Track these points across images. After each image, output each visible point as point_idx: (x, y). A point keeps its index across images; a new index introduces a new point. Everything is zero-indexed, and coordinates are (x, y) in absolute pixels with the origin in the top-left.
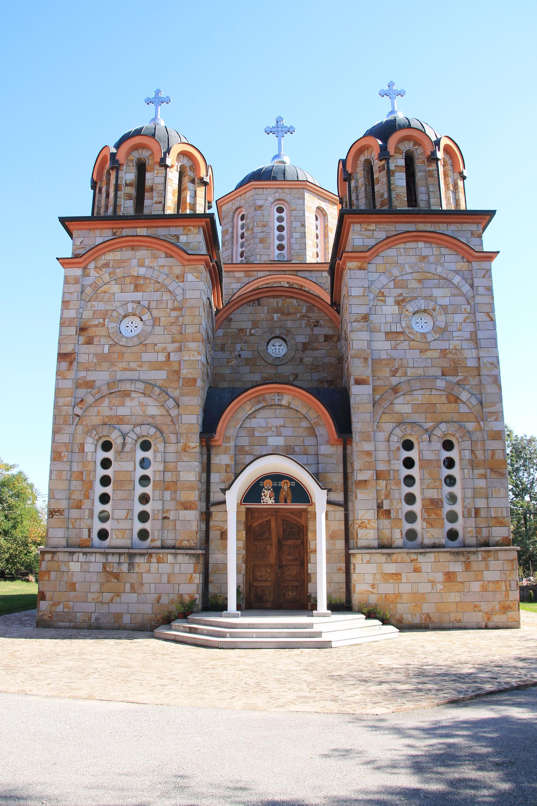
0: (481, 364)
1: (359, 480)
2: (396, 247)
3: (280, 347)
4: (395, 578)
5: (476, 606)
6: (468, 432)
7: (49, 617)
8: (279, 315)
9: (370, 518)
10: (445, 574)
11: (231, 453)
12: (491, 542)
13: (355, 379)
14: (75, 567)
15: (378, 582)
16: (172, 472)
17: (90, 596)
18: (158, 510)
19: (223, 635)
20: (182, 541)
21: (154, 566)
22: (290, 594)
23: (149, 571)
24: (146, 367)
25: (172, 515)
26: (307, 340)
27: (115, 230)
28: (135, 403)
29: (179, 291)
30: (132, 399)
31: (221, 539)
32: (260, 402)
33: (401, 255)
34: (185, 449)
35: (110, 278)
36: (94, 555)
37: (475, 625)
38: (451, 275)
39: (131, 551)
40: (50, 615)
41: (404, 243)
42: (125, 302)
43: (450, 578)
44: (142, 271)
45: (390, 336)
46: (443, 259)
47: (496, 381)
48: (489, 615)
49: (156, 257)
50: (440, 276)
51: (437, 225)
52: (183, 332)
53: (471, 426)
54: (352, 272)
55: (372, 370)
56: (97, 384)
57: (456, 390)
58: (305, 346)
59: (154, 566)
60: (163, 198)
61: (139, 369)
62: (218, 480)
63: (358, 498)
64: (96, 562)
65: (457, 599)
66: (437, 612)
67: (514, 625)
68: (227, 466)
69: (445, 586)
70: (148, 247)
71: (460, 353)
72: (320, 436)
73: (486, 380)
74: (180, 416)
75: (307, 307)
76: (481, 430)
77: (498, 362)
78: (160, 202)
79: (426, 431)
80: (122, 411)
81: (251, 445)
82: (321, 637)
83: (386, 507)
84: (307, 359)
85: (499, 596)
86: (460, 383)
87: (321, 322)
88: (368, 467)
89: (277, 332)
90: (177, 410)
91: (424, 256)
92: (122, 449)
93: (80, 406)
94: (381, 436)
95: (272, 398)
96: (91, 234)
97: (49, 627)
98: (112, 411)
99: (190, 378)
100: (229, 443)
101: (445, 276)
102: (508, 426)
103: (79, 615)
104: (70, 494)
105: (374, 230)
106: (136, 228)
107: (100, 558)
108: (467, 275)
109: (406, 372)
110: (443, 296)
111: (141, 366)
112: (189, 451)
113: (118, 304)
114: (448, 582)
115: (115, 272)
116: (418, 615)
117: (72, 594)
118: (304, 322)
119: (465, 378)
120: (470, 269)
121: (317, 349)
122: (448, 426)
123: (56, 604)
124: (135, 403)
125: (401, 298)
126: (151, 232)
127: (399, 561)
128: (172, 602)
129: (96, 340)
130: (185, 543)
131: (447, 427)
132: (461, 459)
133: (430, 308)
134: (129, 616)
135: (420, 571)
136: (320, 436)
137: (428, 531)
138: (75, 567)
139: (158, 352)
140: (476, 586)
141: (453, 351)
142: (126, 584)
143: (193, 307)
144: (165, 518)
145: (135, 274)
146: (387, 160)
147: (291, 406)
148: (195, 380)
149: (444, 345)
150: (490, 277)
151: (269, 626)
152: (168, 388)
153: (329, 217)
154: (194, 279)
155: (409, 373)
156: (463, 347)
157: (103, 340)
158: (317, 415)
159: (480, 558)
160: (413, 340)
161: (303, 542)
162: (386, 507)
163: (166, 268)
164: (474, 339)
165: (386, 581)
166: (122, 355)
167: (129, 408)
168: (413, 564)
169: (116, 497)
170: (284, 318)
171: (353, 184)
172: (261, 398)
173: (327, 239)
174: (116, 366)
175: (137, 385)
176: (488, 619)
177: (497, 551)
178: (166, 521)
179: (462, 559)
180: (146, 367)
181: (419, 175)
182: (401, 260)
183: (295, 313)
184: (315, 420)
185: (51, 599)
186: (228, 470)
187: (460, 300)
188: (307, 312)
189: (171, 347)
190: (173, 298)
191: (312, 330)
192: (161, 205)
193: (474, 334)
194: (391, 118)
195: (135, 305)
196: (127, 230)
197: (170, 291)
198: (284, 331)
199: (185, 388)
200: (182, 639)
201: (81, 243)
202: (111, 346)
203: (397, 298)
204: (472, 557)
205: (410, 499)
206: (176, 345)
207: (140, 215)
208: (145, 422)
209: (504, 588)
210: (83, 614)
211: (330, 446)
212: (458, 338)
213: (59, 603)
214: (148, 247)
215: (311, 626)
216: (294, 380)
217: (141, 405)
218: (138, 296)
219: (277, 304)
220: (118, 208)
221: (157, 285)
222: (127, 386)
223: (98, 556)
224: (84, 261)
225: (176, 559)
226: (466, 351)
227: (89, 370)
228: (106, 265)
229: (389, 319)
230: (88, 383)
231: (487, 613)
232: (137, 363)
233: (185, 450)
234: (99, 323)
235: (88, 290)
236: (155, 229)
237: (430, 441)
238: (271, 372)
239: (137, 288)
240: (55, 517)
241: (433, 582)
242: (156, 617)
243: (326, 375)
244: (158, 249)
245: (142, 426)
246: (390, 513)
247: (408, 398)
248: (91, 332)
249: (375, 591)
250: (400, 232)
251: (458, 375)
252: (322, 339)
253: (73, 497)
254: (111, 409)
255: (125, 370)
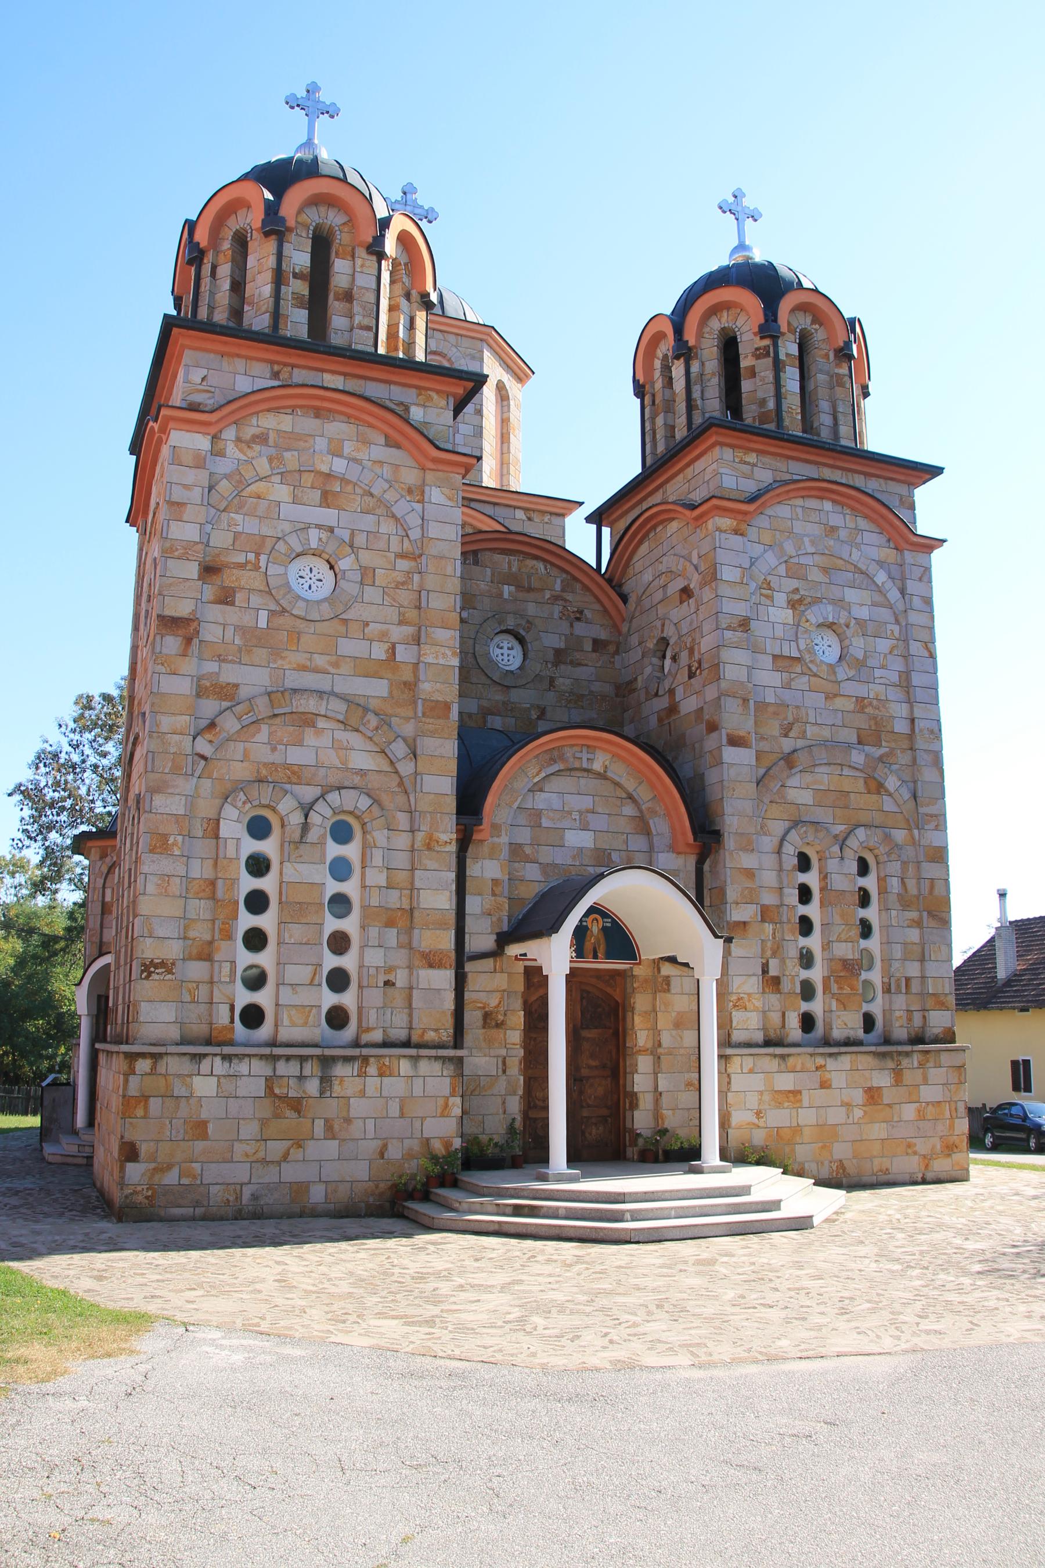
0: (917, 731)
1: (735, 922)
2: (790, 502)
3: (510, 652)
4: (792, 1099)
5: (909, 1146)
6: (897, 845)
7: (147, 1197)
8: (512, 588)
9: (751, 991)
10: (865, 1092)
11: (502, 857)
12: (927, 1035)
13: (728, 735)
14: (204, 1086)
15: (767, 1107)
16: (401, 889)
17: (239, 1149)
18: (377, 967)
19: (617, 1217)
20: (424, 1030)
21: (372, 1083)
22: (594, 1131)
23: (362, 1094)
24: (346, 668)
25: (401, 979)
26: (562, 645)
27: (276, 368)
28: (325, 740)
29: (414, 520)
30: (319, 732)
31: (484, 1027)
32: (555, 762)
33: (798, 519)
34: (430, 845)
35: (272, 469)
36: (247, 1060)
37: (907, 1178)
38: (873, 568)
39: (328, 1052)
40: (150, 1193)
41: (803, 497)
42: (303, 526)
43: (872, 1097)
44: (339, 465)
45: (780, 663)
46: (859, 537)
47: (937, 761)
48: (927, 1159)
49: (367, 443)
50: (855, 566)
51: (849, 474)
52: (424, 604)
53: (899, 836)
54: (723, 536)
55: (756, 723)
56: (244, 692)
57: (880, 772)
58: (560, 656)
59: (372, 1083)
60: (374, 321)
61: (333, 671)
62: (478, 911)
63: (733, 954)
64: (252, 1077)
65: (884, 1135)
66: (854, 1157)
67: (960, 1177)
68: (495, 882)
69: (865, 1112)
70: (349, 416)
71: (884, 706)
72: (658, 834)
73: (923, 758)
74: (419, 777)
75: (562, 581)
76: (914, 843)
77: (940, 730)
78: (368, 328)
79: (836, 836)
80: (296, 756)
81: (535, 843)
82: (779, 1209)
83: (773, 972)
84: (561, 680)
85: (942, 1128)
86: (884, 760)
87: (588, 614)
88: (750, 898)
89: (511, 623)
90: (412, 764)
91: (832, 527)
92: (302, 837)
93: (208, 736)
94: (768, 843)
95: (578, 755)
96: (225, 363)
97: (148, 1220)
98: (276, 753)
99: (438, 701)
100: (499, 836)
101: (864, 568)
102: (18, 781)
103: (214, 1190)
104: (186, 928)
105: (754, 465)
106: (323, 371)
107: (260, 1068)
108: (895, 571)
109: (805, 732)
110: (859, 602)
111: (336, 665)
112: (437, 848)
113: (287, 527)
114: (870, 1104)
115: (282, 457)
116: (826, 1163)
117: (200, 1145)
118: (557, 609)
119: (891, 753)
120: (899, 561)
121: (580, 664)
122: (869, 833)
123: (164, 1168)
124: (325, 740)
125: (797, 597)
126: (352, 385)
127: (798, 1068)
128: (409, 1156)
129: (239, 597)
130: (431, 1036)
131: (867, 835)
132: (821, 890)
133: (842, 621)
134: (322, 1187)
135: (829, 1087)
136: (658, 834)
137: (839, 1017)
138: (204, 1086)
139: (371, 641)
140: (909, 1112)
141: (875, 702)
142: (317, 1121)
143: (441, 558)
144: (387, 983)
145: (324, 468)
146: (775, 338)
147: (609, 774)
148: (447, 706)
149: (861, 690)
150: (930, 581)
151: (680, 1195)
152: (391, 716)
153: (512, 403)
154: (443, 500)
155: (809, 734)
156: (889, 698)
157: (256, 600)
158: (652, 796)
159: (916, 1064)
160: (815, 675)
161: (616, 1033)
162: (773, 972)
163: (386, 468)
164: (905, 683)
165: (779, 1105)
166: (296, 636)
167: (316, 749)
168: (819, 1073)
169: (291, 937)
170: (521, 595)
171: (695, 367)
172: (556, 753)
173: (505, 445)
174: (283, 658)
175: (331, 703)
176: (927, 1166)
177: (939, 1051)
178: (390, 990)
179: (891, 1064)
180: (346, 668)
181: (820, 379)
182: (799, 527)
183: (542, 590)
184: (649, 805)
185: (152, 1158)
186: (498, 891)
187: (885, 614)
188: (563, 590)
189: (398, 633)
190: (401, 532)
191: (572, 626)
192: (371, 335)
193: (904, 676)
194: (739, 258)
195: (324, 535)
196: (304, 372)
197: (394, 516)
198: (523, 623)
199: (428, 720)
200: (520, 1230)
201: (203, 379)
202: (272, 613)
203: (792, 596)
204: (905, 1062)
205: (806, 959)
206: (409, 630)
207: (318, 343)
208: (346, 784)
209: (947, 1115)
210: (223, 1187)
211: (674, 855)
212: (882, 681)
213: (170, 1167)
214: (349, 416)
215: (745, 1190)
216: (539, 718)
217: (337, 746)
218: (328, 516)
219: (510, 567)
220: (281, 321)
221: (367, 499)
222: (311, 705)
223: (255, 1062)
224: (217, 422)
225: (416, 1067)
226: (892, 705)
227: (224, 661)
228: (262, 439)
229: (779, 632)
230: (222, 688)
231: (924, 1156)
232: (328, 658)
233: (429, 847)
234: (247, 562)
235: (224, 486)
236: (362, 382)
237: (842, 858)
238: (498, 698)
239: (327, 499)
240: (154, 976)
241: (848, 1105)
242: (377, 1187)
243: (595, 716)
244: (371, 426)
245: (343, 791)
246: (779, 983)
247: (808, 778)
248: (229, 578)
249: (761, 1123)
250: (795, 477)
251: (881, 746)
252: (588, 646)
253: (192, 934)
254: (274, 749)
255: (303, 668)
